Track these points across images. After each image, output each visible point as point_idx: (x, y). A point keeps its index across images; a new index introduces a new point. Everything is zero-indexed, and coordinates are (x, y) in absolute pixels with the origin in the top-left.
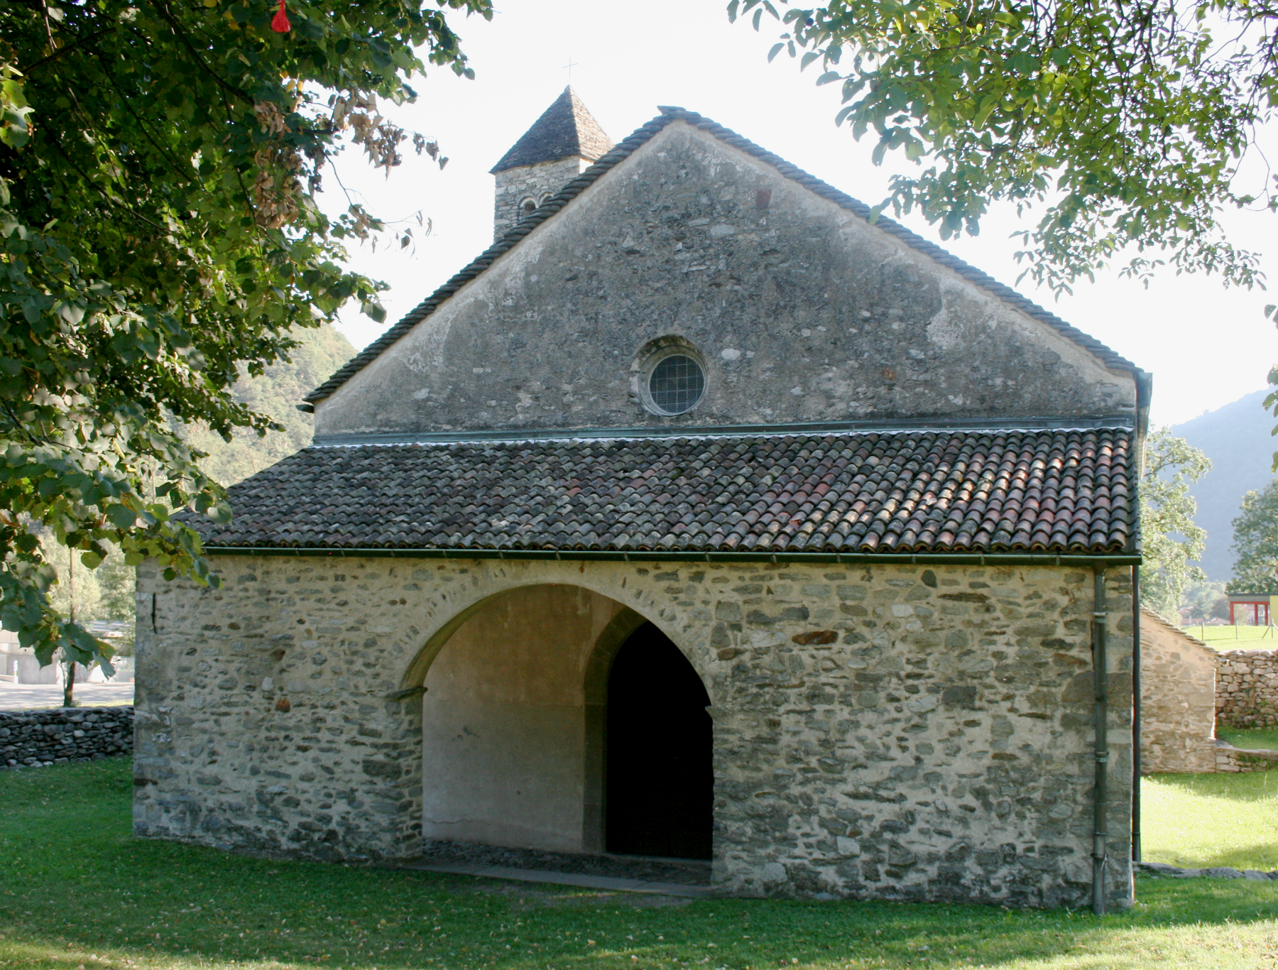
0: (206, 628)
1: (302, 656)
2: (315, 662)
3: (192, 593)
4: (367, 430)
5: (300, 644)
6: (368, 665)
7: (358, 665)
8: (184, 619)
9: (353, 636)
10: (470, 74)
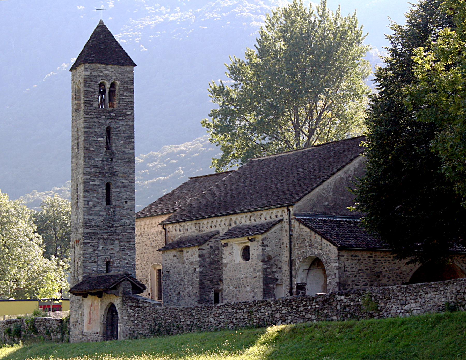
0: (360, 270)
1: (384, 276)
2: (388, 278)
3: (355, 261)
4: (310, 213)
5: (384, 274)
6: (401, 278)
7: (398, 278)
8: (353, 268)
9: (397, 271)
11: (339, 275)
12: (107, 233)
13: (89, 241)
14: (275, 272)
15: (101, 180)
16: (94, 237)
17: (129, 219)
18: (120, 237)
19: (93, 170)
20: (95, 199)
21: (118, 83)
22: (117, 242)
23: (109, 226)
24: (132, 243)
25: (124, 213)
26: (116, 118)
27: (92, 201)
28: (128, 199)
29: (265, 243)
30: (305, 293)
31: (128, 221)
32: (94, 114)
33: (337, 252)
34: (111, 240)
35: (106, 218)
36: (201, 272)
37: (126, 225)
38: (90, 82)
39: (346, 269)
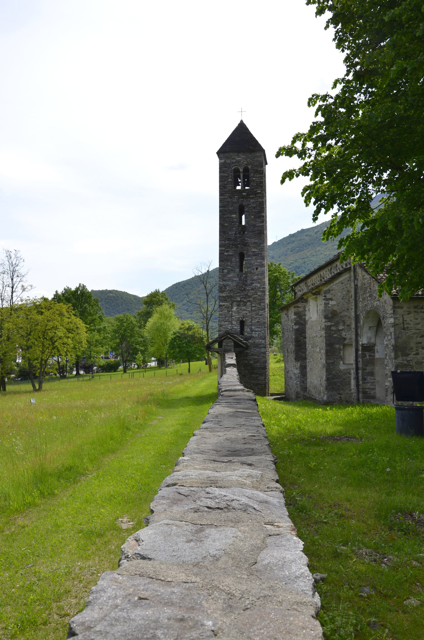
10: (283, 182)
11: (395, 335)
12: (240, 296)
13: (224, 304)
14: (342, 330)
15: (235, 250)
16: (228, 300)
17: (259, 283)
18: (251, 299)
19: (227, 242)
20: (229, 267)
21: (250, 167)
22: (248, 304)
23: (241, 290)
24: (262, 304)
25: (255, 278)
27: (226, 269)
28: (258, 265)
29: (328, 296)
30: (374, 356)
31: (258, 285)
32: (228, 195)
33: (391, 302)
34: (243, 302)
35: (239, 283)
37: (257, 288)
38: (224, 169)
39: (406, 326)
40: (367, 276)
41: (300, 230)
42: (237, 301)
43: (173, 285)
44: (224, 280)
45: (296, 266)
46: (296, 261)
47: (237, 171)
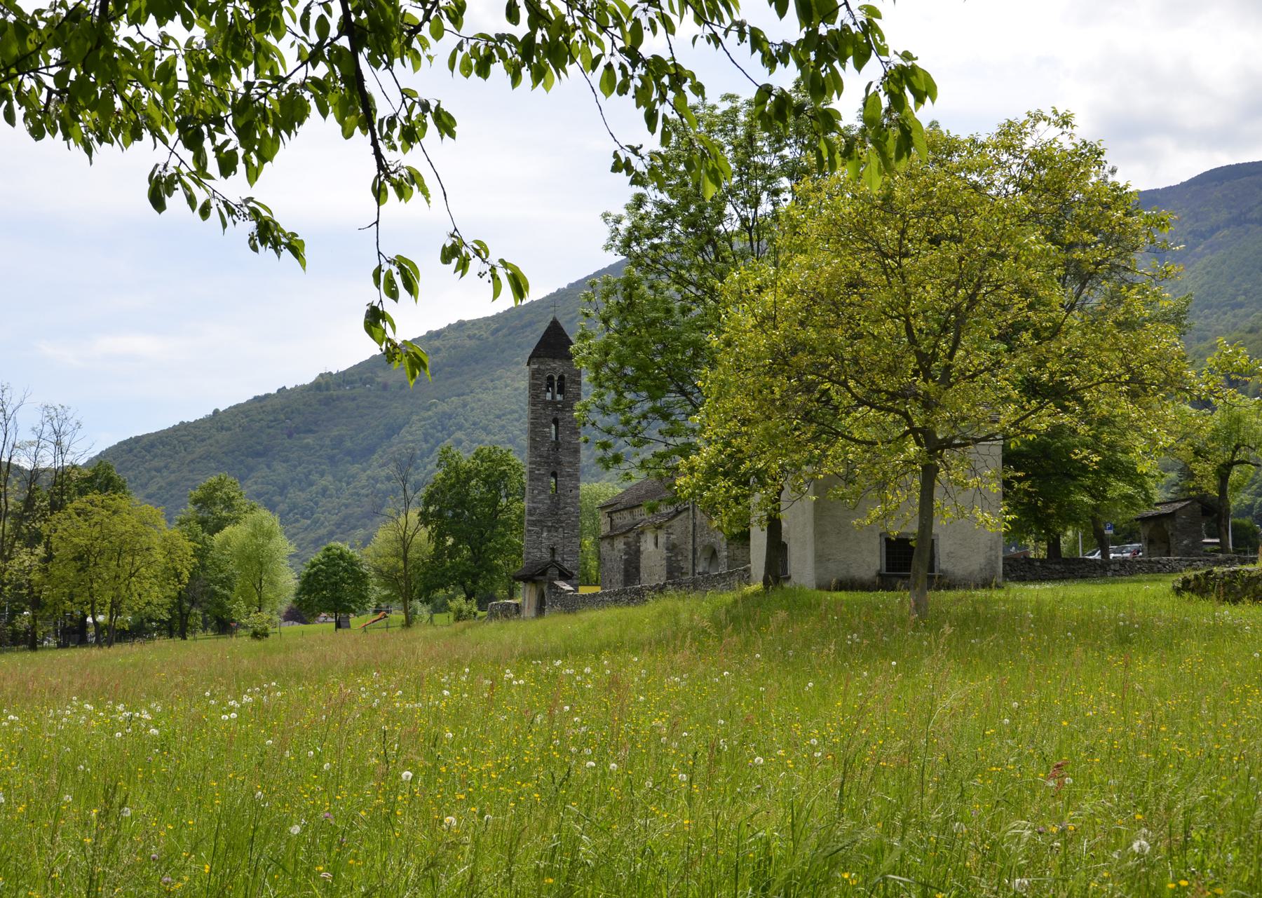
21: (566, 376)
26: (562, 410)
29: (670, 531)
36: (626, 560)
40: (705, 517)
41: (454, 321)
42: (548, 527)
43: (121, 444)
44: (533, 502)
45: (444, 413)
46: (443, 401)
47: (550, 378)
